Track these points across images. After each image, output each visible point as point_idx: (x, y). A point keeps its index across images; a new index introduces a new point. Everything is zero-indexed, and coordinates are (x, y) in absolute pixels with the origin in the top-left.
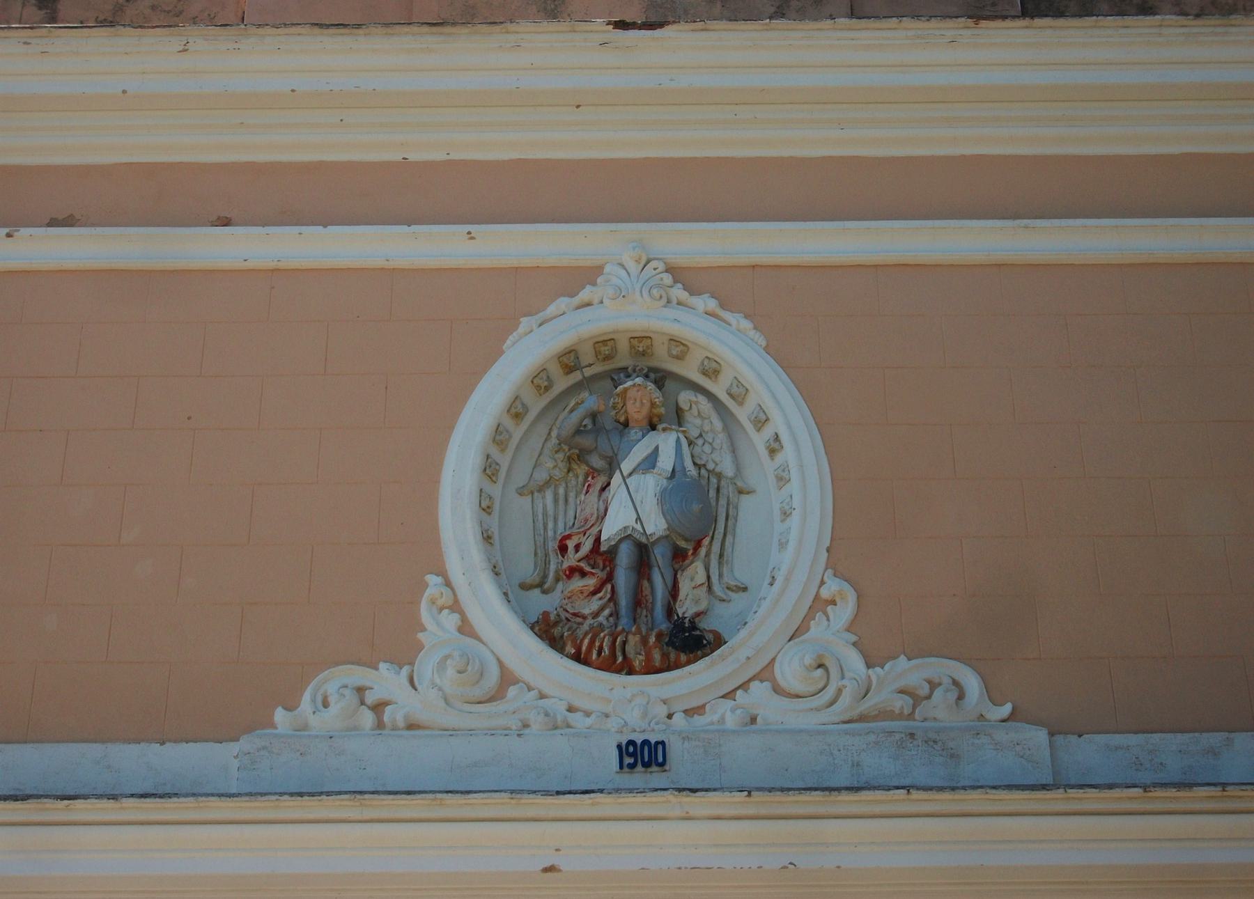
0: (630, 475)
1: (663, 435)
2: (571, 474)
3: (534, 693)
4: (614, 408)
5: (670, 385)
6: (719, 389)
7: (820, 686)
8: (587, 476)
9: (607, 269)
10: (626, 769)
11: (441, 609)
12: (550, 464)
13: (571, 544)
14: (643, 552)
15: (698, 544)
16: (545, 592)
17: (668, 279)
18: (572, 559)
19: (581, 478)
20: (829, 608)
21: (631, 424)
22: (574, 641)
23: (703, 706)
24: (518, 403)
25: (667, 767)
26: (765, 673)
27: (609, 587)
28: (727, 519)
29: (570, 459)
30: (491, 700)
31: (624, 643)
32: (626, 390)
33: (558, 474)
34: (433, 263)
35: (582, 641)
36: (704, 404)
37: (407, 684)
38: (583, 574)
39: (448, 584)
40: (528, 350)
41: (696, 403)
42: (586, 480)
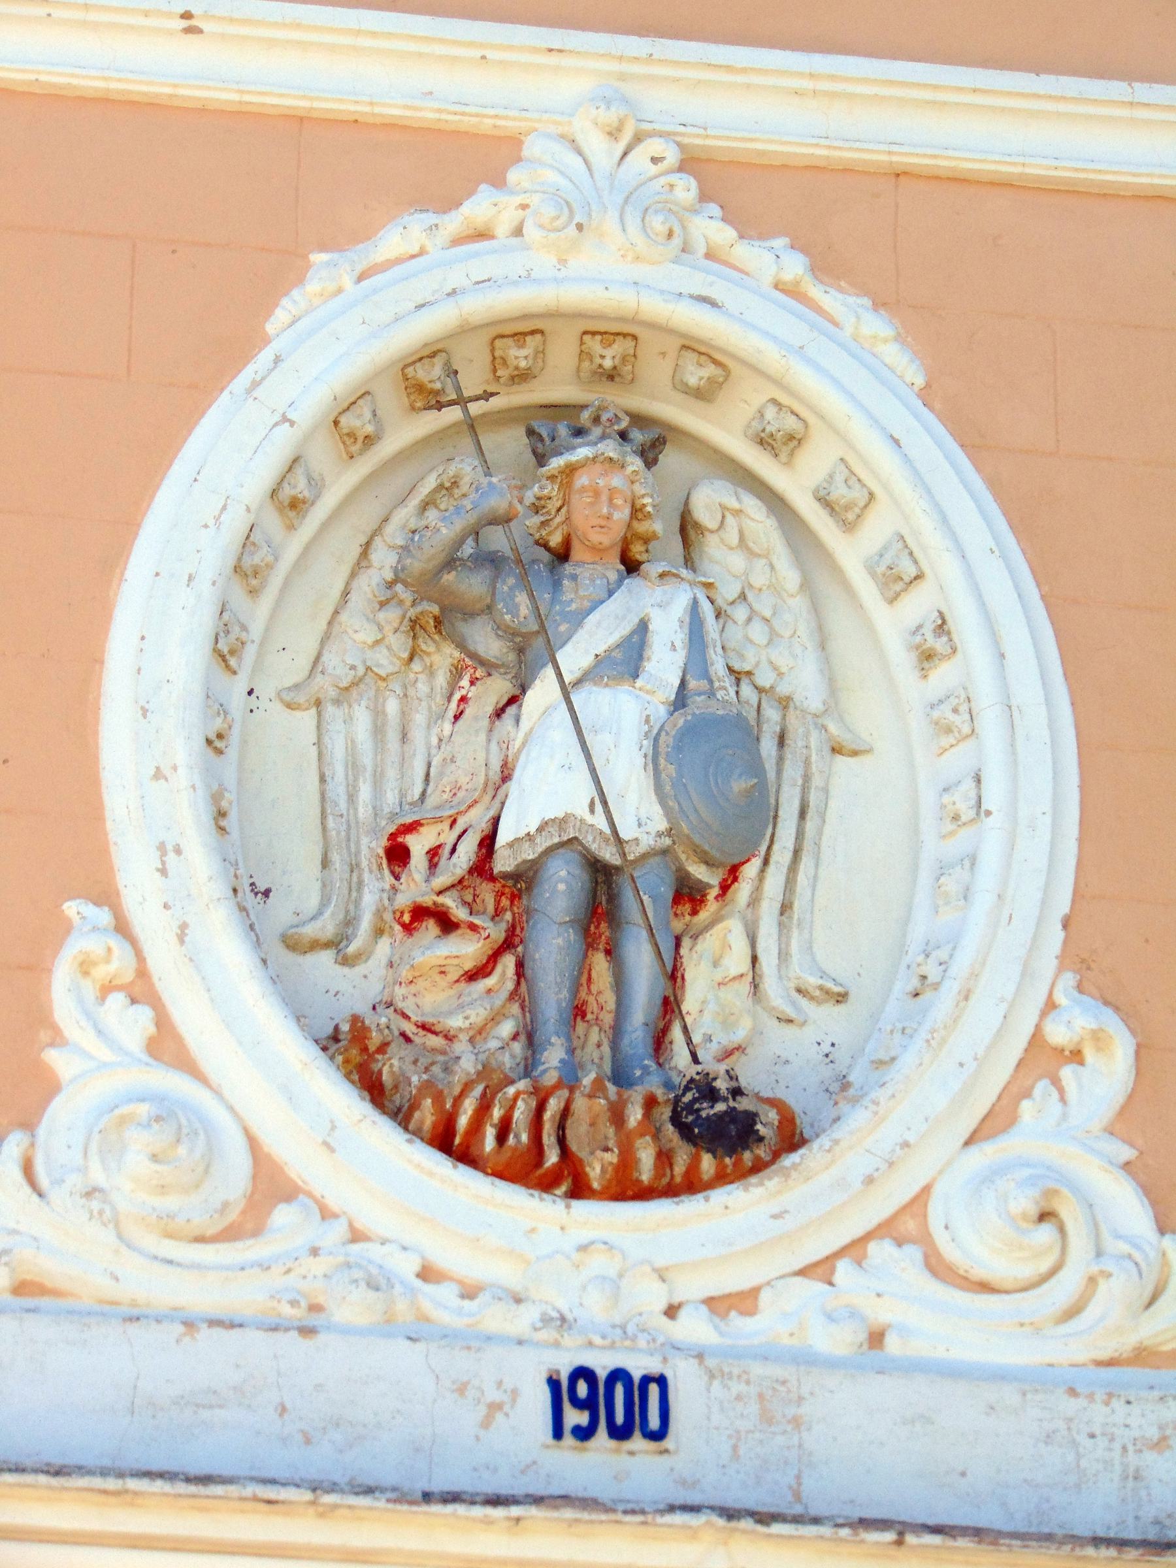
0: (578, 683)
1: (659, 592)
2: (416, 666)
3: (339, 1229)
4: (536, 509)
5: (670, 458)
6: (795, 483)
7: (1045, 1265)
8: (457, 672)
9: (533, 147)
10: (569, 1440)
11: (106, 990)
12: (367, 635)
13: (418, 845)
14: (603, 881)
15: (734, 872)
16: (346, 961)
17: (686, 189)
18: (418, 885)
19: (442, 679)
20: (1067, 1073)
21: (577, 553)
22: (438, 1098)
23: (754, 1292)
24: (299, 471)
25: (668, 1443)
26: (907, 1224)
27: (508, 963)
28: (803, 814)
29: (415, 625)
30: (229, 1234)
31: (566, 1113)
32: (571, 470)
33: (384, 662)
34: (90, 82)
35: (458, 1100)
36: (758, 520)
37: (17, 1175)
38: (447, 925)
39: (122, 928)
40: (336, 330)
41: (738, 513)
42: (453, 686)
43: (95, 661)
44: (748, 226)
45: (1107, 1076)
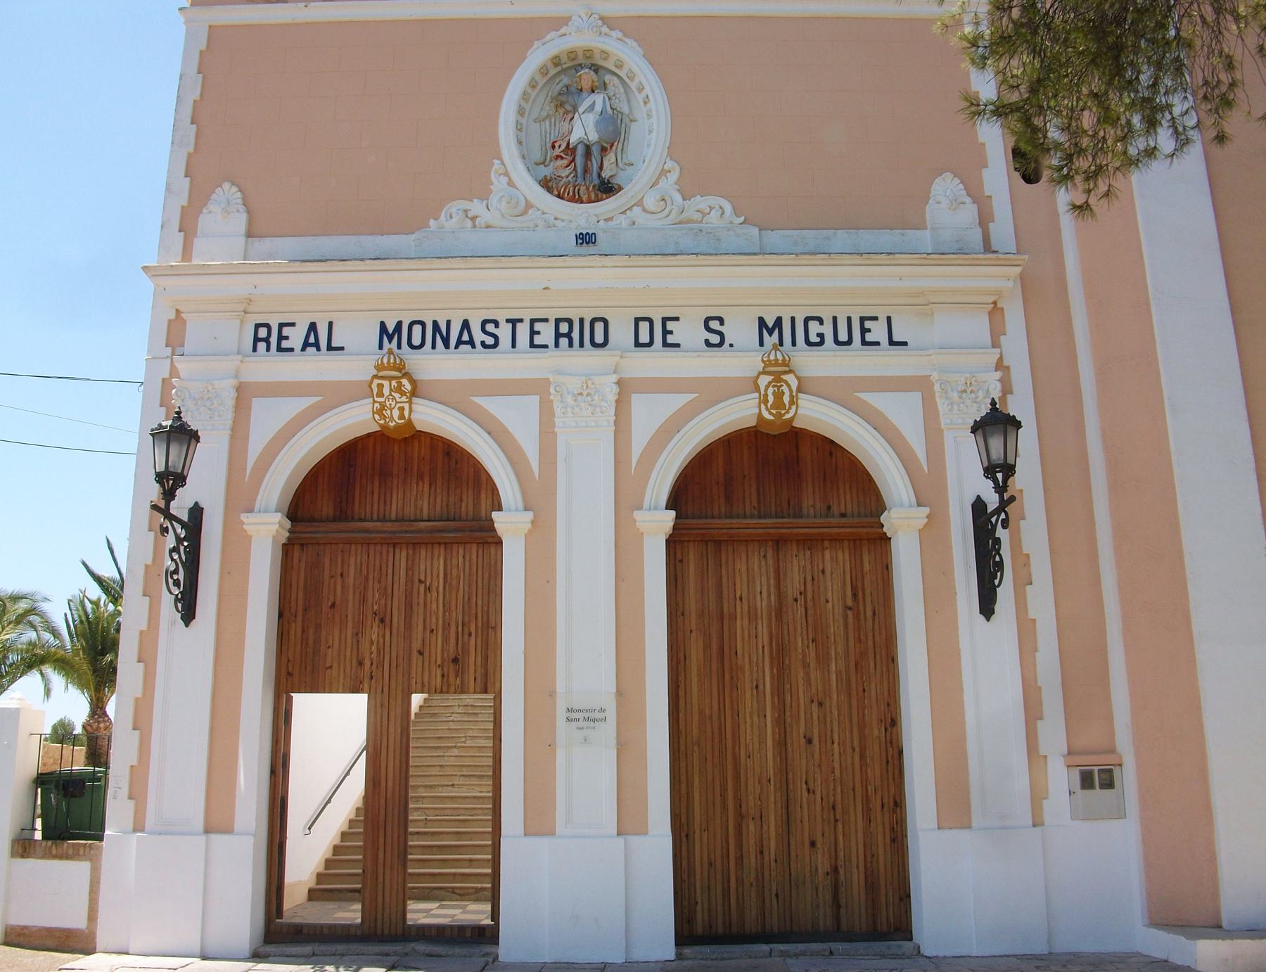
6: (622, 74)
14: (588, 149)
17: (600, 23)
18: (557, 151)
26: (640, 203)
36: (616, 80)
43: (497, 118)
44: (611, 29)
45: (674, 176)
